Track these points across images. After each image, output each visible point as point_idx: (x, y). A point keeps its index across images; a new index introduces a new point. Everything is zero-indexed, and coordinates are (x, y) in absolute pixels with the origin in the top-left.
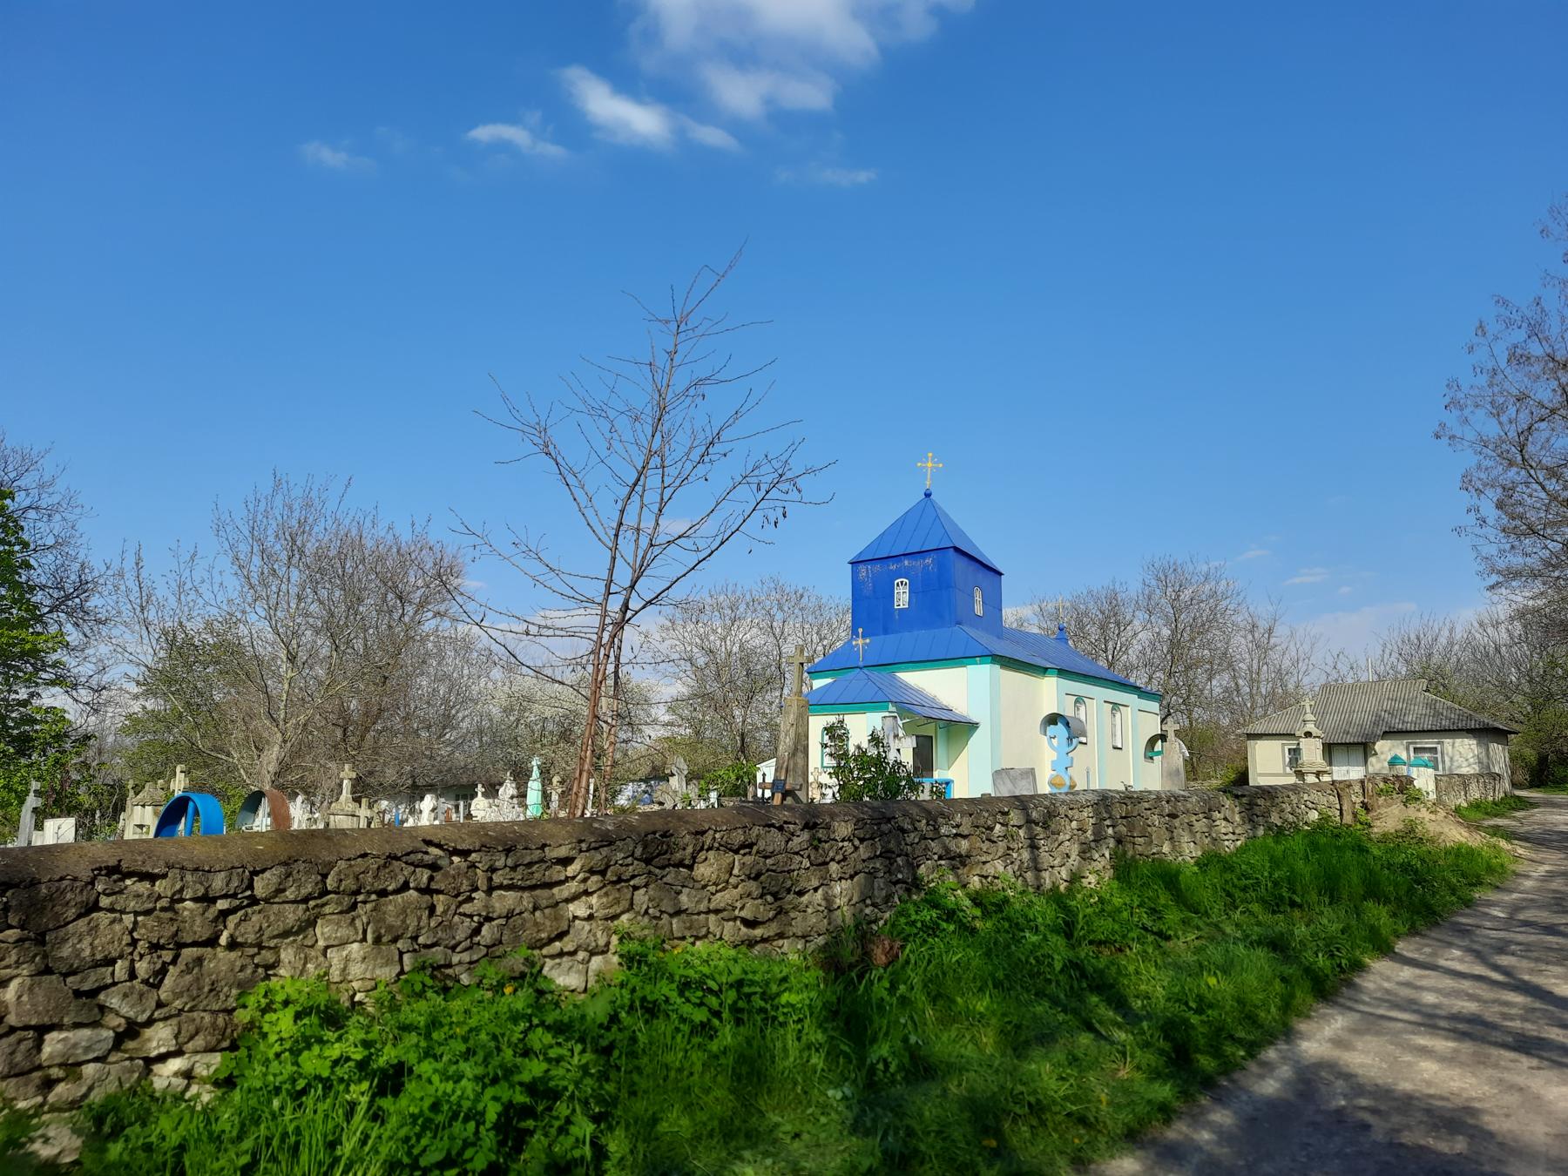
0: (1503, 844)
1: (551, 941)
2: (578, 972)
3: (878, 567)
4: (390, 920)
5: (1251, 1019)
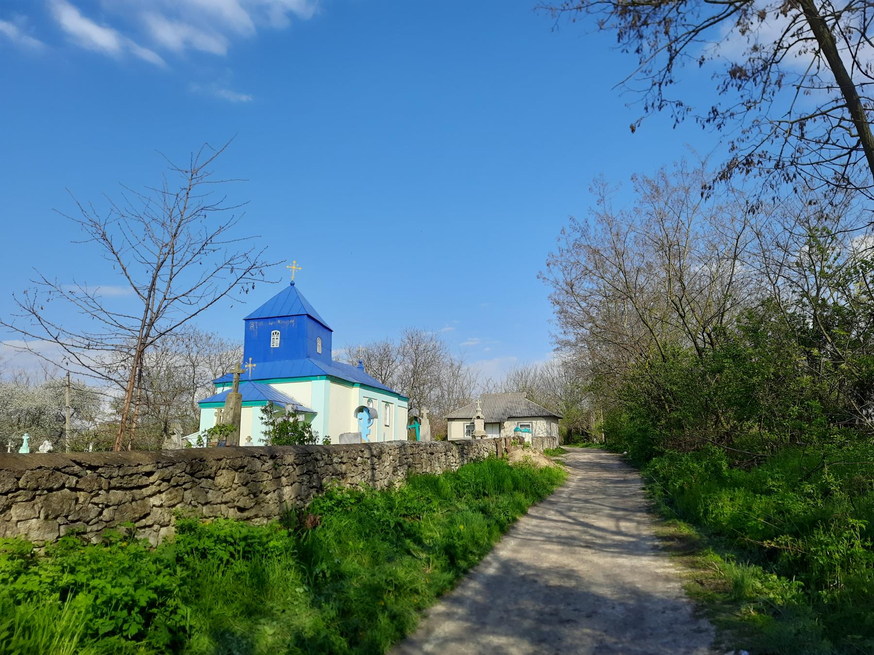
0: (562, 467)
1: (141, 518)
2: (154, 536)
3: (261, 323)
4: (54, 506)
5: (477, 544)
